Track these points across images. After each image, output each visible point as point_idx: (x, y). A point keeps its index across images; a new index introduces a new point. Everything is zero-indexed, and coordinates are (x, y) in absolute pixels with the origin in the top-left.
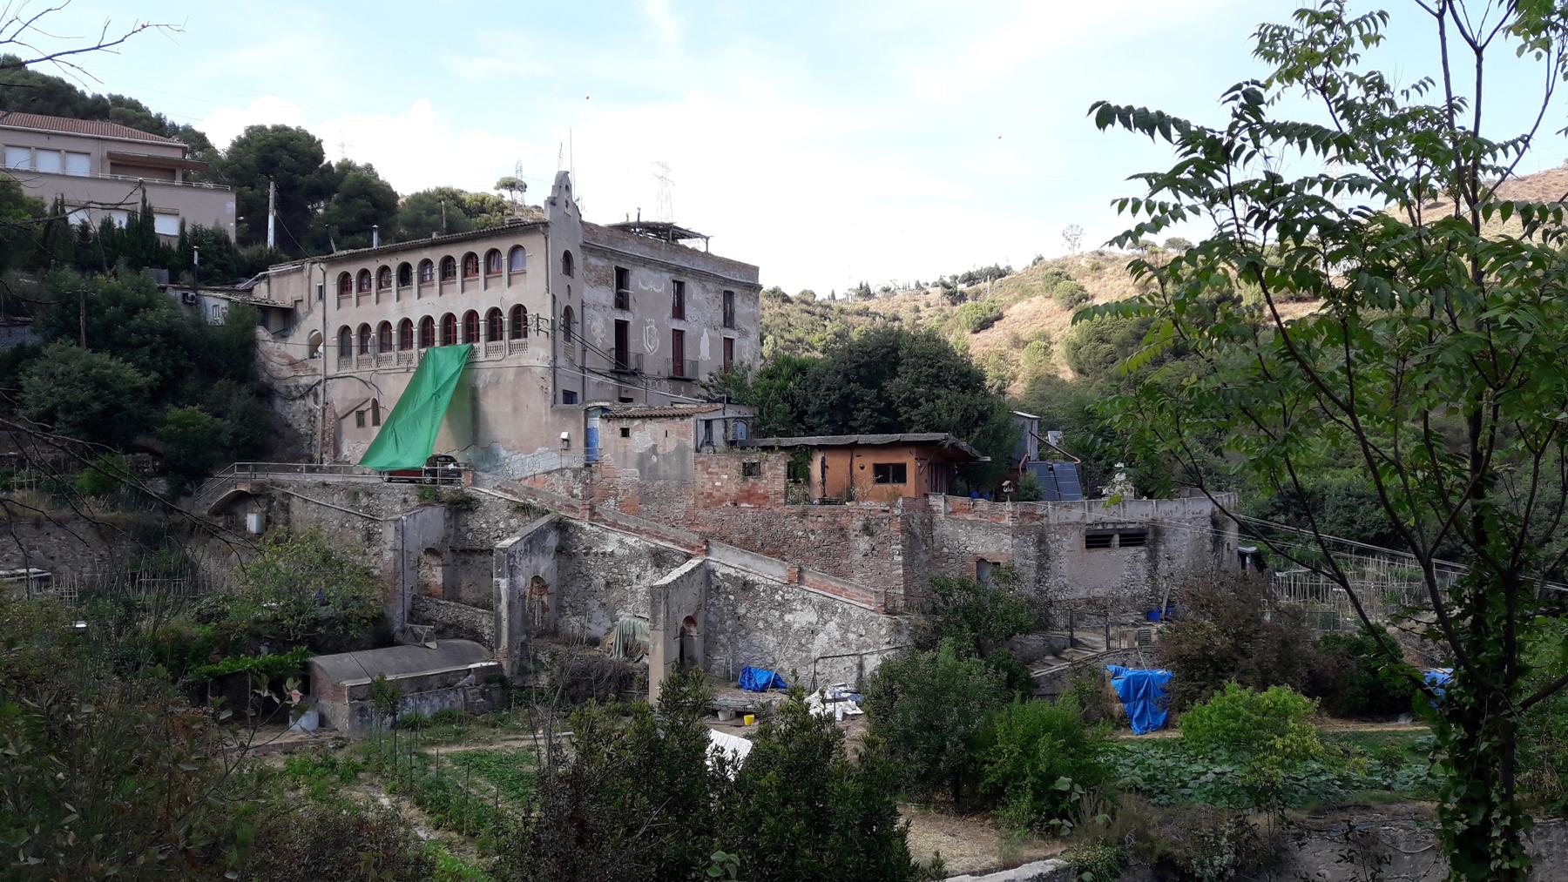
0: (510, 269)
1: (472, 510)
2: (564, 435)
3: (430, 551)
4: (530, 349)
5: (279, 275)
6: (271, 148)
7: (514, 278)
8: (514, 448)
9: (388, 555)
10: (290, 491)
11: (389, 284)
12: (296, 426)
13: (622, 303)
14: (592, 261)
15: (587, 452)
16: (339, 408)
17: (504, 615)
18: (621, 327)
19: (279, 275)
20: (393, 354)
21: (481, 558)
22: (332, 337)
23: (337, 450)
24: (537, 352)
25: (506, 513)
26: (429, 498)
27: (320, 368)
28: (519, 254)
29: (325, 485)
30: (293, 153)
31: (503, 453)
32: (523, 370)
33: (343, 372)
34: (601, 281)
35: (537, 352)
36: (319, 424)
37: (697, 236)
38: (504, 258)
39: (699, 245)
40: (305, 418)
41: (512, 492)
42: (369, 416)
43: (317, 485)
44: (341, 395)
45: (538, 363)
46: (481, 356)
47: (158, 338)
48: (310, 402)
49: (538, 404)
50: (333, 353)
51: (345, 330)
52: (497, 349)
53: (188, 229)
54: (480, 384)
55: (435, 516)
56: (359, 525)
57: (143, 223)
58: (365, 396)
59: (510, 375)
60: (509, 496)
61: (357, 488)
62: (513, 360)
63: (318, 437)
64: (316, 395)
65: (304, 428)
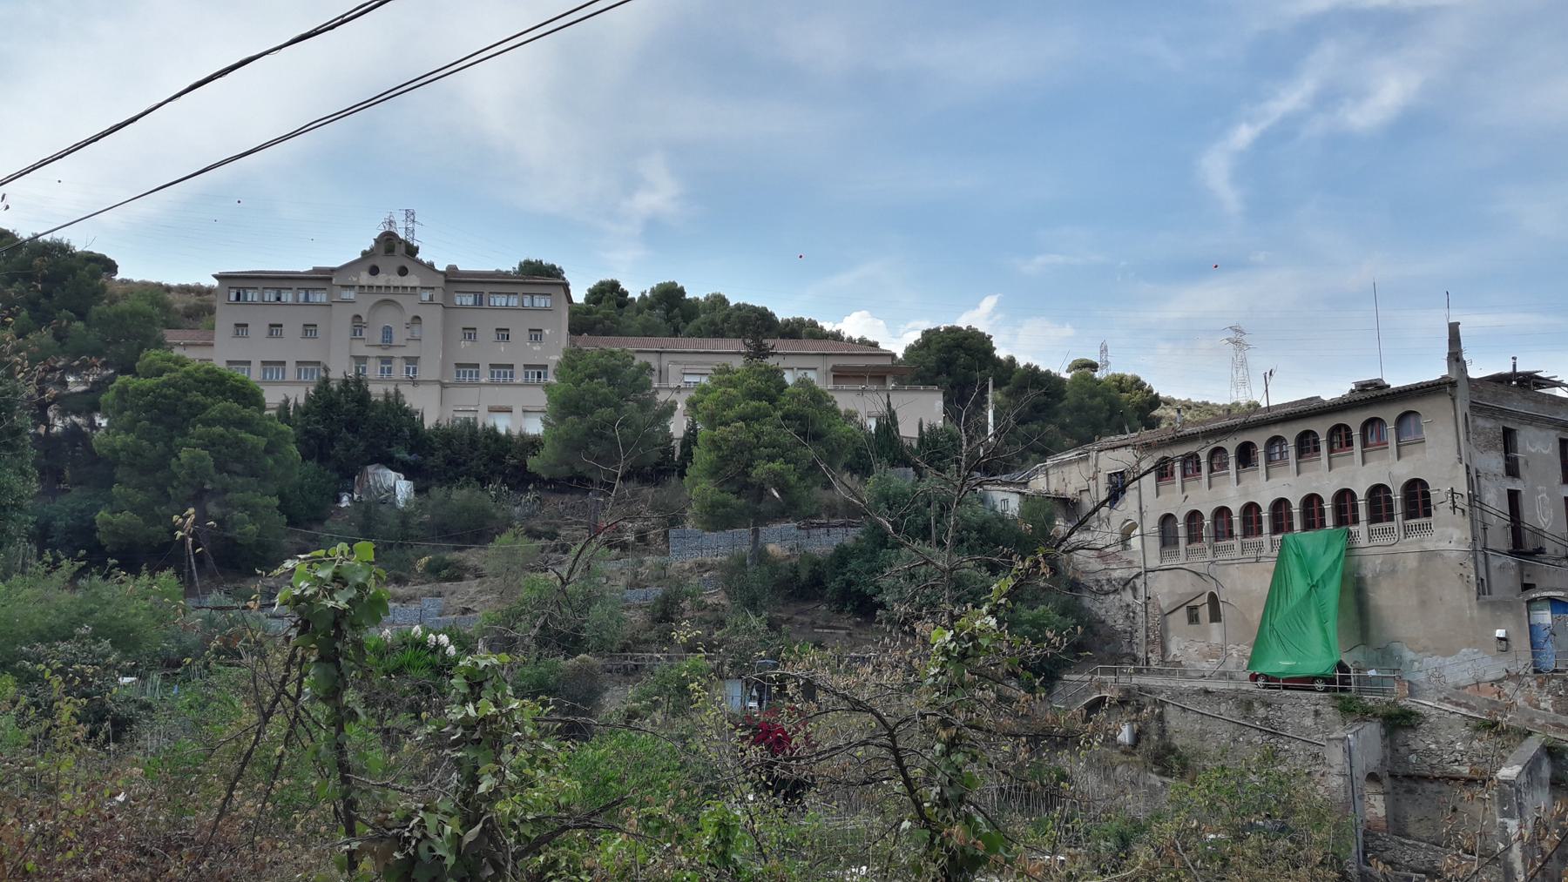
0: (1398, 440)
1: (1413, 727)
2: (1500, 633)
3: (1372, 777)
4: (1437, 531)
5: (1056, 466)
6: (949, 349)
7: (1404, 450)
8: (1425, 649)
9: (1336, 782)
10: (1162, 697)
11: (1225, 466)
12: (1110, 622)
13: (1512, 470)
14: (1480, 422)
15: (1534, 655)
16: (1165, 603)
17: (1518, 866)
18: (1513, 496)
19: (1056, 466)
20: (1236, 543)
21: (1434, 787)
22: (1151, 524)
23: (1164, 649)
24: (1448, 534)
25: (1465, 732)
26: (1350, 710)
27: (1138, 560)
28: (1412, 419)
29: (1207, 692)
30: (969, 351)
31: (1409, 655)
32: (1428, 556)
33: (1167, 564)
34: (1490, 446)
35: (1448, 534)
36: (1140, 620)
37: (1559, 384)
38: (1391, 427)
39: (1559, 392)
40: (1122, 613)
41: (1467, 706)
42: (1204, 612)
43: (1197, 692)
44: (1166, 588)
45: (1452, 546)
46: (1362, 540)
47: (974, 534)
48: (1127, 596)
49: (1457, 596)
50: (1154, 543)
51: (1167, 519)
52: (1384, 531)
53: (925, 428)
54: (1368, 573)
55: (1367, 740)
56: (1257, 739)
57: (888, 424)
58: (1199, 590)
59: (1412, 562)
60: (1464, 711)
61: (1250, 697)
62: (1413, 544)
63: (1141, 633)
64: (1134, 589)
65: (1120, 625)
